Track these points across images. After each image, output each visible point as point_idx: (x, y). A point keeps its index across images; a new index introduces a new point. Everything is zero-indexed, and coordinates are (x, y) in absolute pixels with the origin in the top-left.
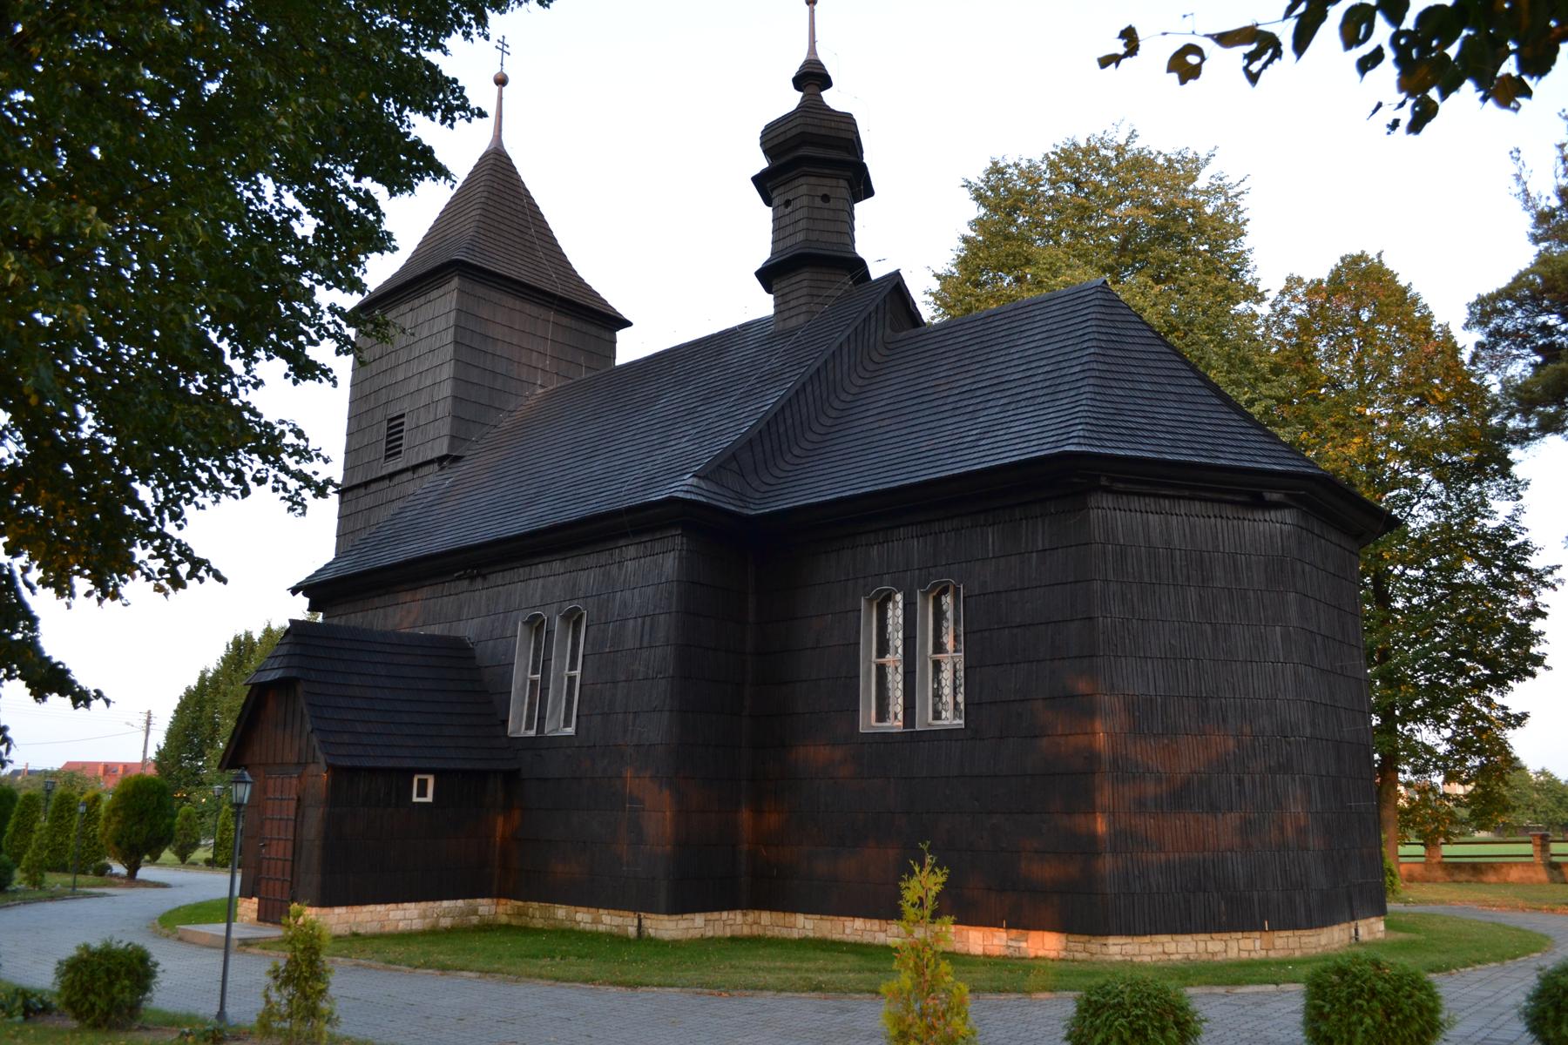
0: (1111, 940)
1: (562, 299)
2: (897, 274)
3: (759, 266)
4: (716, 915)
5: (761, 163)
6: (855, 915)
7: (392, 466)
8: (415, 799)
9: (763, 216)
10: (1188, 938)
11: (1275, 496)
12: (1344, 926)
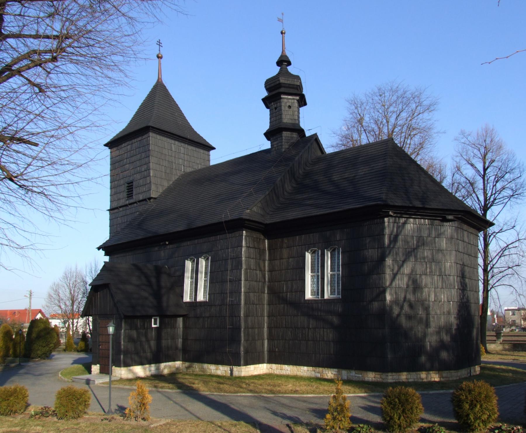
0: (390, 374)
1: (189, 140)
2: (316, 134)
3: (265, 131)
4: (257, 366)
5: (265, 94)
6: (304, 365)
7: (131, 201)
8: (153, 326)
9: (267, 112)
10: (414, 373)
11: (450, 217)
12: (466, 369)
